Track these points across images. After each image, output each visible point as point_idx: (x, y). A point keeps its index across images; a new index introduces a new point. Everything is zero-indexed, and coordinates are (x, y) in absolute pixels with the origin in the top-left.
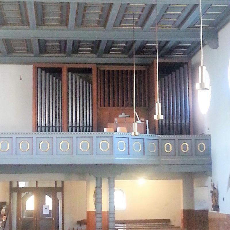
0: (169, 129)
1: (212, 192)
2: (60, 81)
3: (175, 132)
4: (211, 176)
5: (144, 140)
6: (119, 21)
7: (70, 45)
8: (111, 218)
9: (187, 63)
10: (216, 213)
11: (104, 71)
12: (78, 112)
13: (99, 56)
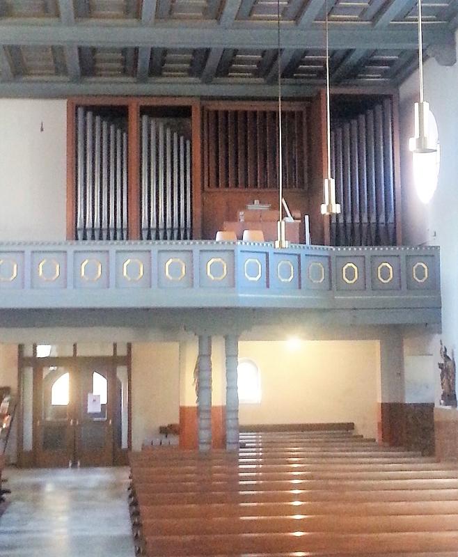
1: (441, 366)
2: (124, 135)
4: (440, 332)
6: (246, 9)
7: (144, 58)
9: (390, 97)
11: (216, 112)
13: (207, 81)
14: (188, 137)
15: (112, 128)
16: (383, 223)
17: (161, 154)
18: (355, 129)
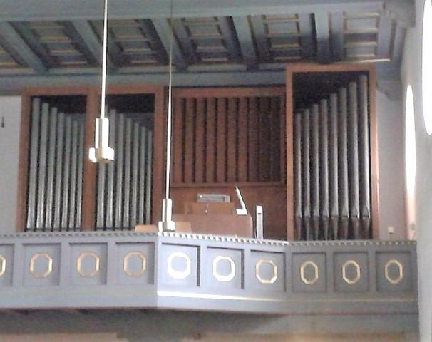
0: (321, 226)
2: (150, 133)
3: (317, 236)
5: (199, 250)
12: (210, 157)
16: (336, 216)
18: (325, 110)
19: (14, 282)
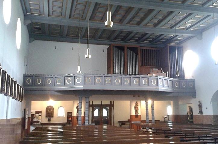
1: (199, 105)
8: (128, 124)
10: (200, 115)
14: (137, 54)
15: (132, 52)
17: (118, 56)
19: (141, 85)
